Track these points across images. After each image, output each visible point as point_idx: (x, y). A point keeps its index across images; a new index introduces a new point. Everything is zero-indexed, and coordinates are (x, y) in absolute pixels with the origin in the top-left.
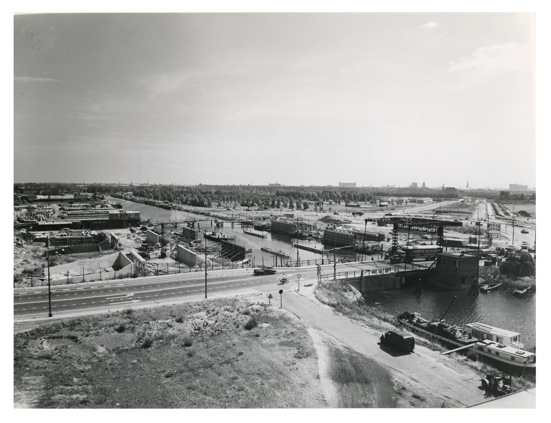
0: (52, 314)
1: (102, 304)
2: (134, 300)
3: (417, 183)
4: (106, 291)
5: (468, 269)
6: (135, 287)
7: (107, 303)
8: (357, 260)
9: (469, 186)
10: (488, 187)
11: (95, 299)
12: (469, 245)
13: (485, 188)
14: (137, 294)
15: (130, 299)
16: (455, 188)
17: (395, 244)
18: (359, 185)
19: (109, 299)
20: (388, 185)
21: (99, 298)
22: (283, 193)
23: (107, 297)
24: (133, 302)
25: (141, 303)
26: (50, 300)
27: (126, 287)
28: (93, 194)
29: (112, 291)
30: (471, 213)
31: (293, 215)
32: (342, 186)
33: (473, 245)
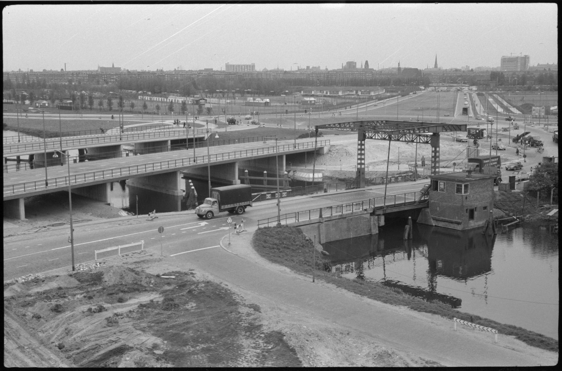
3: (356, 63)
5: (478, 196)
9: (439, 66)
10: (467, 66)
13: (462, 67)
16: (419, 69)
17: (361, 164)
18: (259, 68)
20: (308, 67)
22: (337, 85)
31: (515, 177)
32: (231, 71)
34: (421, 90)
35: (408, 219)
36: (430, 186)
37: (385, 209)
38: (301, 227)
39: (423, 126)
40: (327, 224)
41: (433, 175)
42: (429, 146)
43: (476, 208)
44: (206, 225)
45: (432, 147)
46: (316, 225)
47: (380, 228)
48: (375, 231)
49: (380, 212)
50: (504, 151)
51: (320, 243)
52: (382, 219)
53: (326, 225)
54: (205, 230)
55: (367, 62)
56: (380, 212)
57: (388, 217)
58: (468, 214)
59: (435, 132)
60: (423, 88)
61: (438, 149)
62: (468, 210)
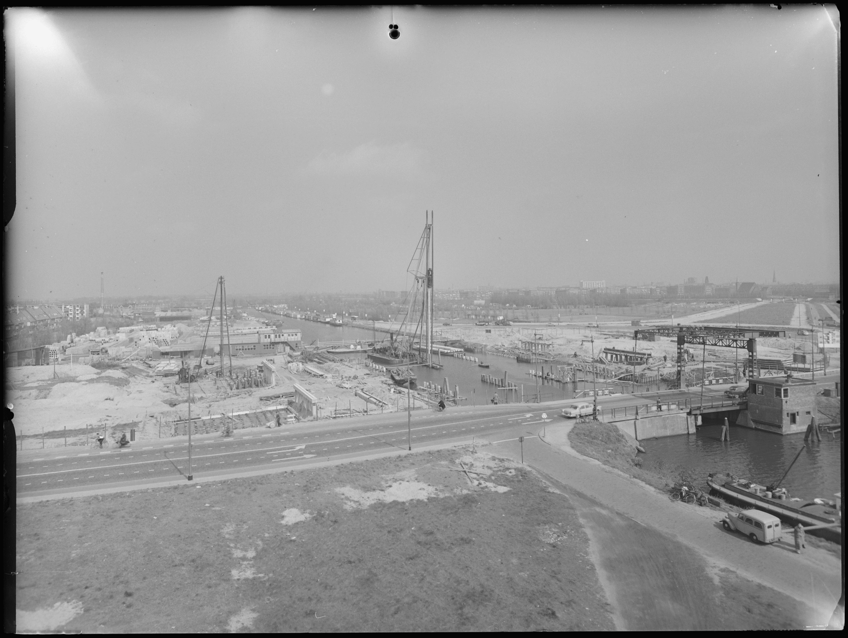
0: (192, 476)
1: (261, 461)
2: (307, 454)
4: (265, 441)
5: (799, 401)
6: (306, 435)
7: (270, 459)
8: (625, 391)
11: (251, 453)
12: (793, 366)
14: (312, 446)
15: (694, 396)
19: (272, 454)
21: (257, 453)
23: (268, 451)
24: (305, 458)
25: (317, 458)
26: (409, 429)
27: (293, 437)
28: (232, 308)
29: (274, 442)
30: (785, 336)
33: (801, 366)
34: (759, 301)
35: (725, 420)
36: (748, 389)
37: (702, 409)
38: (617, 424)
39: (741, 331)
40: (643, 421)
41: (750, 378)
42: (746, 351)
43: (798, 412)
44: (531, 417)
45: (749, 352)
46: (633, 421)
47: (697, 427)
48: (693, 430)
49: (698, 412)
50: (487, 370)
51: (636, 439)
52: (700, 418)
53: (642, 422)
54: (529, 421)
55: (707, 278)
56: (698, 412)
57: (705, 417)
58: (789, 418)
59: (751, 338)
60: (760, 299)
61: (755, 354)
62: (789, 414)
